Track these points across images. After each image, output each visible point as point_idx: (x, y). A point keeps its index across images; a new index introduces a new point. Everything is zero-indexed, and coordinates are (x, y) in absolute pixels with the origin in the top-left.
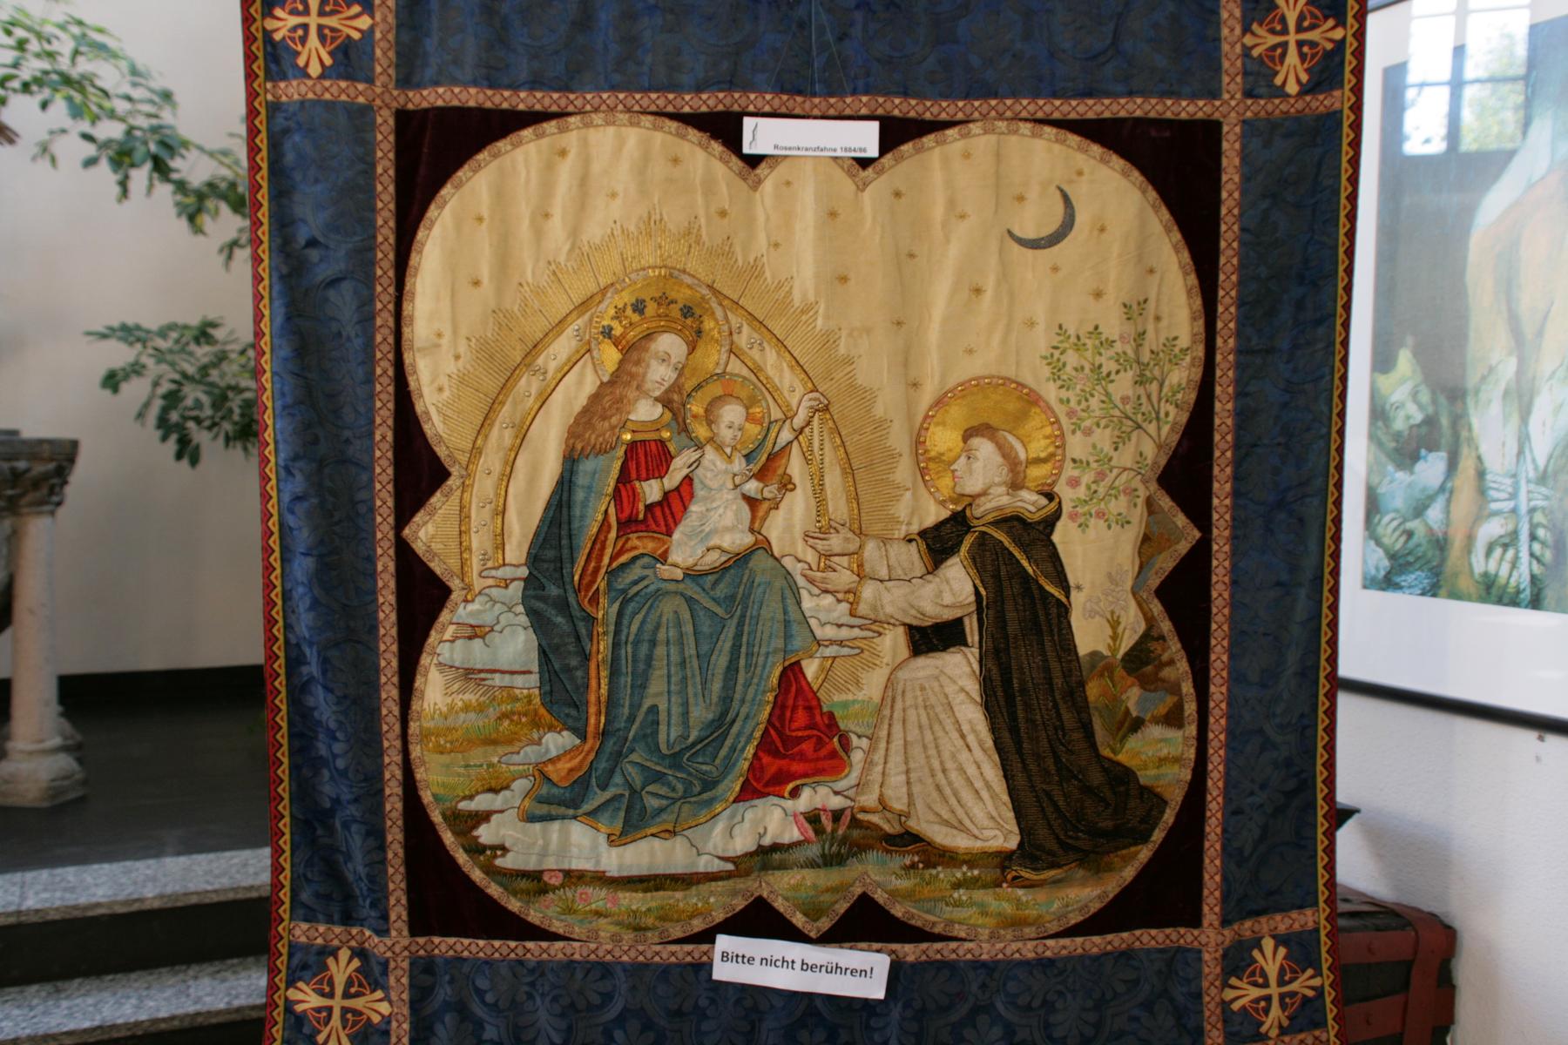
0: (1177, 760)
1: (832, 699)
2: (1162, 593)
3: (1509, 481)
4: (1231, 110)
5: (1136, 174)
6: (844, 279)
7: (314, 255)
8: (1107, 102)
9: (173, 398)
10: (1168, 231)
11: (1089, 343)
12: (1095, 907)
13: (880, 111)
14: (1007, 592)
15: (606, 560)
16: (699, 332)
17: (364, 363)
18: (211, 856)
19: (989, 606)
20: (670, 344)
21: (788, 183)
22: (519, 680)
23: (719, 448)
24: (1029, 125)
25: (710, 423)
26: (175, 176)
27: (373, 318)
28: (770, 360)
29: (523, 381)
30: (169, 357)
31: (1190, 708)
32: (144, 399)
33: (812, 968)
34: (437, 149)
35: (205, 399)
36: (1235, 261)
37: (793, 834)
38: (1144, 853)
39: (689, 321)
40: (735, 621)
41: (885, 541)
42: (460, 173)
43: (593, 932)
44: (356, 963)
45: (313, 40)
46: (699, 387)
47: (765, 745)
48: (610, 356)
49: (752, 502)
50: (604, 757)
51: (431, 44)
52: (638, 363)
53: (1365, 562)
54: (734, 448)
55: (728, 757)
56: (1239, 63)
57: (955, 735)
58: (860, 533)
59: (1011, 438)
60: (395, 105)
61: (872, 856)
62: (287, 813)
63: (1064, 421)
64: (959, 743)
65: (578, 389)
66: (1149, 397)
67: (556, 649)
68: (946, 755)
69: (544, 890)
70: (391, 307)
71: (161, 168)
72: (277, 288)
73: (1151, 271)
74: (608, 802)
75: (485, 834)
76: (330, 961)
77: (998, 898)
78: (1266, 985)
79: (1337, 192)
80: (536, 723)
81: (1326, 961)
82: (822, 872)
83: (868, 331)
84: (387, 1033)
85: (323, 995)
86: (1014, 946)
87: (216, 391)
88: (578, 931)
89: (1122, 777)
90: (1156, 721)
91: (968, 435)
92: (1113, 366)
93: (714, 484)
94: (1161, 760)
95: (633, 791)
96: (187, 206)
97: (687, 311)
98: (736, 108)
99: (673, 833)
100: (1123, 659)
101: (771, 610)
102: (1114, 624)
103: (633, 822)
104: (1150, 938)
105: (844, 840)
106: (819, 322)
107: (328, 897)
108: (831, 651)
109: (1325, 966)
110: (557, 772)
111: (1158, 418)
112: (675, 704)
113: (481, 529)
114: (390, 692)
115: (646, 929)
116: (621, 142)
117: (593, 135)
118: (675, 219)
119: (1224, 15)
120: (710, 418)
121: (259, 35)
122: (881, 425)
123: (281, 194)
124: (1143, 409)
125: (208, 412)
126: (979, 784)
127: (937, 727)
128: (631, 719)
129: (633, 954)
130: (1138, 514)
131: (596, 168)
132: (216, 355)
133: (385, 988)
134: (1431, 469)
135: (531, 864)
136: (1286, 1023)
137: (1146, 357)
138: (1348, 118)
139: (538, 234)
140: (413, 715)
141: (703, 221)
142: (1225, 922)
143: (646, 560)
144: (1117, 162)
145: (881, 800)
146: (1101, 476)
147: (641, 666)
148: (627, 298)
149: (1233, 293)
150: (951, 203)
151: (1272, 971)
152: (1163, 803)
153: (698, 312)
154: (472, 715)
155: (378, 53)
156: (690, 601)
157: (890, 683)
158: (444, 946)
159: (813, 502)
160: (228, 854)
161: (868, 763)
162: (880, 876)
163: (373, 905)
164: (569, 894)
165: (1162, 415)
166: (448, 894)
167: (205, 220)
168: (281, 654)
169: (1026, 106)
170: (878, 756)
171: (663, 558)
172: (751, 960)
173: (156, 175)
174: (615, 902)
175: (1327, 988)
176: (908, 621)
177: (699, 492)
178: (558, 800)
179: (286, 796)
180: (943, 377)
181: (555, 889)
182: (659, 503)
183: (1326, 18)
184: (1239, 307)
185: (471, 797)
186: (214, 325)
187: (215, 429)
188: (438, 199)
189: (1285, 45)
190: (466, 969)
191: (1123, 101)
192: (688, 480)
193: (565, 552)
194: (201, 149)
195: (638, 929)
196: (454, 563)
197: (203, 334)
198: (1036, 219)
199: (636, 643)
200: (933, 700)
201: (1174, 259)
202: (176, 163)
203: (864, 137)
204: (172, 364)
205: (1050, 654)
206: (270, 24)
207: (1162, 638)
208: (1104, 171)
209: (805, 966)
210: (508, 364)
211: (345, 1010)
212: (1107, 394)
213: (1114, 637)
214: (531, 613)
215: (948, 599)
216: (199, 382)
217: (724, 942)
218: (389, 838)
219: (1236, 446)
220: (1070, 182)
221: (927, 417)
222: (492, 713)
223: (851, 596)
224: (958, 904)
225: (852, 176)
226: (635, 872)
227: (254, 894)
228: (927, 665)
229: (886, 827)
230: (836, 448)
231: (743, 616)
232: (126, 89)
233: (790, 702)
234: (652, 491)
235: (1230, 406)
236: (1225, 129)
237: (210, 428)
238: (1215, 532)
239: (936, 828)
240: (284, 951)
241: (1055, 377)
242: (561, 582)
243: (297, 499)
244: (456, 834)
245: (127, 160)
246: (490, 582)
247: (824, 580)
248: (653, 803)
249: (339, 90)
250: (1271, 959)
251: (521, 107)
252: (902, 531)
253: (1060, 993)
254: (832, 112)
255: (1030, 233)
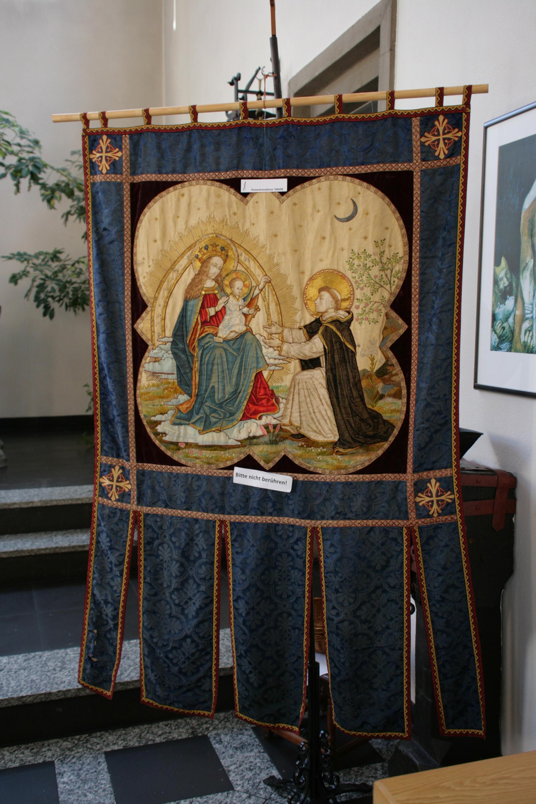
0: (398, 411)
1: (272, 384)
2: (392, 348)
3: (531, 306)
4: (416, 166)
5: (380, 192)
6: (276, 236)
7: (105, 233)
8: (369, 166)
9: (41, 287)
10: (394, 213)
11: (362, 256)
12: (367, 464)
13: (288, 175)
14: (335, 348)
15: (197, 335)
16: (227, 256)
17: (121, 269)
18: (62, 488)
19: (328, 353)
20: (217, 260)
21: (257, 202)
22: (170, 377)
23: (235, 296)
24: (341, 177)
25: (231, 288)
26: (41, 181)
27: (124, 254)
28: (253, 266)
29: (171, 275)
30: (40, 268)
31: (404, 392)
32: (28, 288)
33: (266, 480)
34: (144, 195)
35: (56, 287)
36: (419, 223)
37: (259, 433)
38: (386, 445)
39: (223, 252)
40: (240, 357)
41: (291, 329)
42: (150, 204)
43: (195, 464)
44: (121, 471)
45: (104, 161)
46: (227, 275)
47: (250, 401)
48: (198, 264)
49: (246, 315)
50: (198, 403)
51: (140, 160)
52: (206, 267)
53: (491, 340)
54: (239, 296)
55: (238, 405)
56: (419, 148)
57: (318, 400)
58: (282, 326)
59: (335, 291)
60: (130, 181)
61: (287, 442)
62: (99, 420)
63: (354, 284)
64: (319, 402)
65: (188, 277)
66: (386, 275)
67: (182, 366)
68: (315, 407)
69: (179, 449)
70: (130, 250)
71: (34, 178)
72: (94, 245)
73: (387, 228)
74: (199, 419)
75: (159, 429)
76: (113, 470)
77: (332, 459)
78: (431, 496)
79: (457, 196)
80: (176, 391)
81: (456, 489)
82: (269, 446)
83: (284, 254)
84: (130, 495)
85: (110, 480)
86: (338, 477)
87: (61, 283)
88: (189, 464)
89: (376, 416)
90: (390, 396)
91: (321, 290)
92: (371, 264)
93: (233, 309)
94: (392, 411)
95: (207, 416)
96: (47, 196)
97: (223, 249)
98: (239, 176)
99: (220, 431)
100: (376, 372)
101: (252, 353)
102: (372, 359)
103: (207, 426)
104: (389, 477)
105: (278, 435)
106: (268, 251)
107: (112, 448)
108: (273, 368)
109: (455, 491)
110: (183, 408)
111: (390, 283)
112: (221, 386)
113: (157, 325)
114: (130, 380)
115: (211, 464)
116: (201, 190)
117: (193, 188)
118: (218, 217)
119: (414, 131)
120: (231, 285)
121: (88, 160)
122: (290, 287)
123: (95, 213)
124: (384, 280)
125: (57, 293)
126: (326, 418)
127: (311, 397)
128: (206, 390)
129: (207, 472)
130: (382, 319)
131: (193, 200)
132: (61, 266)
133: (129, 480)
134: (510, 302)
135: (175, 440)
136: (440, 511)
137: (384, 260)
138: (462, 166)
139: (175, 224)
140: (138, 388)
141: (228, 217)
142: (415, 471)
143: (210, 335)
144: (373, 188)
145: (290, 421)
146: (367, 305)
147: (209, 372)
148: (203, 244)
149: (418, 236)
150: (314, 206)
151: (434, 491)
152: (393, 427)
153: (227, 249)
154: (155, 388)
155: (124, 164)
156: (225, 350)
157: (293, 379)
158: (148, 467)
159: (266, 315)
160: (69, 487)
161: (286, 408)
162: (291, 449)
163: (125, 451)
164: (187, 451)
165: (392, 282)
166: (149, 450)
167: (55, 202)
168: (97, 367)
169: (341, 170)
170: (289, 406)
171: (216, 335)
172: (246, 476)
173: (32, 181)
174: (201, 454)
175: (456, 499)
176: (300, 358)
177: (228, 312)
178: (183, 418)
179: (99, 414)
180: (312, 270)
181: (182, 449)
182: (214, 316)
183: (454, 129)
184: (420, 241)
185: (155, 416)
186: (60, 252)
187: (61, 302)
188: (143, 213)
189: (438, 140)
190: (155, 475)
191: (375, 166)
192: (224, 307)
193: (185, 333)
194: (52, 168)
195: (209, 464)
196: (149, 336)
197: (55, 256)
198: (344, 211)
199: (208, 364)
200: (310, 387)
201: (397, 223)
202: (41, 175)
203: (282, 184)
204: (41, 271)
205: (349, 370)
206: (92, 156)
207: (393, 365)
208: (368, 192)
209: (264, 479)
210: (167, 268)
211: (117, 486)
212: (369, 275)
213: (372, 364)
214: (174, 354)
215: (315, 350)
216: (53, 279)
217: (237, 470)
218: (130, 429)
219: (420, 293)
220: (356, 197)
221: (307, 284)
222: (162, 387)
223: (279, 348)
224: (319, 461)
225: (278, 198)
226: (207, 444)
227: (80, 502)
228: (308, 373)
229: (292, 432)
230: (273, 296)
231: (243, 355)
232: (18, 140)
233: (259, 386)
234: (212, 311)
235: (417, 278)
236: (415, 173)
237: (59, 301)
238: (413, 326)
239: (311, 433)
240: (99, 466)
241: (351, 269)
242: (183, 342)
243: (100, 314)
244: (151, 428)
245: (19, 174)
246: (161, 343)
247: (270, 343)
248: (213, 420)
249: (112, 178)
250: (434, 487)
251: (169, 180)
252: (298, 326)
253: (354, 495)
254: (271, 176)
255: (342, 216)
